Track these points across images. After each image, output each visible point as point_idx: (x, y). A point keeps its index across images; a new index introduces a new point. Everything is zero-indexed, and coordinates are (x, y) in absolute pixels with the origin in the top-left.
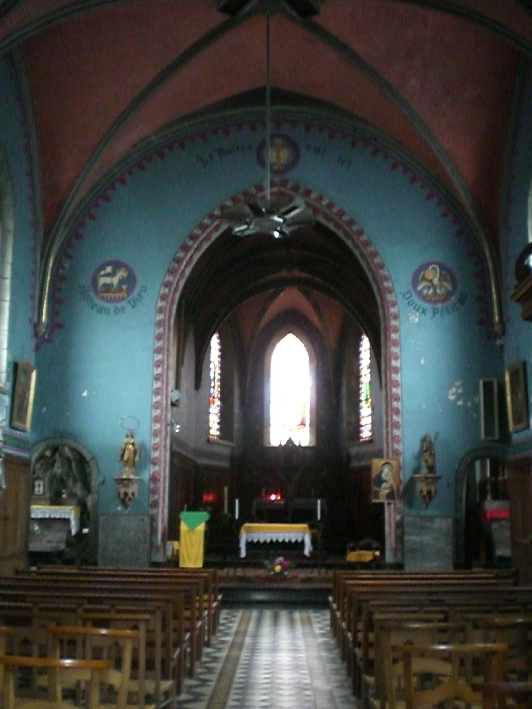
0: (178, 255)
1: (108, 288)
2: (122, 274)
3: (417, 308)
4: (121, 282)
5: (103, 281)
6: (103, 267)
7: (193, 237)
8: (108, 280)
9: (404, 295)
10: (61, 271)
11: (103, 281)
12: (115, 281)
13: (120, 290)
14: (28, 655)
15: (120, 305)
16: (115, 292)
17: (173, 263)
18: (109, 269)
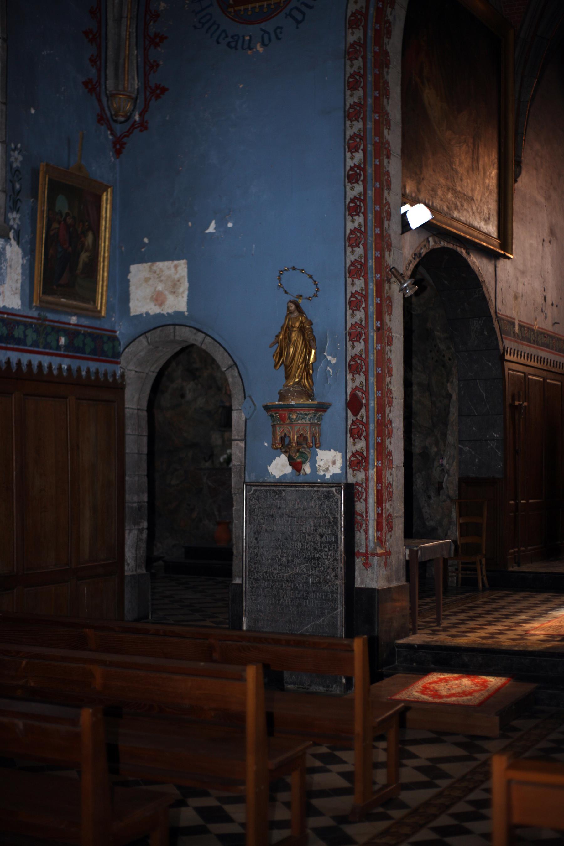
9: (298, 22)
15: (269, 26)
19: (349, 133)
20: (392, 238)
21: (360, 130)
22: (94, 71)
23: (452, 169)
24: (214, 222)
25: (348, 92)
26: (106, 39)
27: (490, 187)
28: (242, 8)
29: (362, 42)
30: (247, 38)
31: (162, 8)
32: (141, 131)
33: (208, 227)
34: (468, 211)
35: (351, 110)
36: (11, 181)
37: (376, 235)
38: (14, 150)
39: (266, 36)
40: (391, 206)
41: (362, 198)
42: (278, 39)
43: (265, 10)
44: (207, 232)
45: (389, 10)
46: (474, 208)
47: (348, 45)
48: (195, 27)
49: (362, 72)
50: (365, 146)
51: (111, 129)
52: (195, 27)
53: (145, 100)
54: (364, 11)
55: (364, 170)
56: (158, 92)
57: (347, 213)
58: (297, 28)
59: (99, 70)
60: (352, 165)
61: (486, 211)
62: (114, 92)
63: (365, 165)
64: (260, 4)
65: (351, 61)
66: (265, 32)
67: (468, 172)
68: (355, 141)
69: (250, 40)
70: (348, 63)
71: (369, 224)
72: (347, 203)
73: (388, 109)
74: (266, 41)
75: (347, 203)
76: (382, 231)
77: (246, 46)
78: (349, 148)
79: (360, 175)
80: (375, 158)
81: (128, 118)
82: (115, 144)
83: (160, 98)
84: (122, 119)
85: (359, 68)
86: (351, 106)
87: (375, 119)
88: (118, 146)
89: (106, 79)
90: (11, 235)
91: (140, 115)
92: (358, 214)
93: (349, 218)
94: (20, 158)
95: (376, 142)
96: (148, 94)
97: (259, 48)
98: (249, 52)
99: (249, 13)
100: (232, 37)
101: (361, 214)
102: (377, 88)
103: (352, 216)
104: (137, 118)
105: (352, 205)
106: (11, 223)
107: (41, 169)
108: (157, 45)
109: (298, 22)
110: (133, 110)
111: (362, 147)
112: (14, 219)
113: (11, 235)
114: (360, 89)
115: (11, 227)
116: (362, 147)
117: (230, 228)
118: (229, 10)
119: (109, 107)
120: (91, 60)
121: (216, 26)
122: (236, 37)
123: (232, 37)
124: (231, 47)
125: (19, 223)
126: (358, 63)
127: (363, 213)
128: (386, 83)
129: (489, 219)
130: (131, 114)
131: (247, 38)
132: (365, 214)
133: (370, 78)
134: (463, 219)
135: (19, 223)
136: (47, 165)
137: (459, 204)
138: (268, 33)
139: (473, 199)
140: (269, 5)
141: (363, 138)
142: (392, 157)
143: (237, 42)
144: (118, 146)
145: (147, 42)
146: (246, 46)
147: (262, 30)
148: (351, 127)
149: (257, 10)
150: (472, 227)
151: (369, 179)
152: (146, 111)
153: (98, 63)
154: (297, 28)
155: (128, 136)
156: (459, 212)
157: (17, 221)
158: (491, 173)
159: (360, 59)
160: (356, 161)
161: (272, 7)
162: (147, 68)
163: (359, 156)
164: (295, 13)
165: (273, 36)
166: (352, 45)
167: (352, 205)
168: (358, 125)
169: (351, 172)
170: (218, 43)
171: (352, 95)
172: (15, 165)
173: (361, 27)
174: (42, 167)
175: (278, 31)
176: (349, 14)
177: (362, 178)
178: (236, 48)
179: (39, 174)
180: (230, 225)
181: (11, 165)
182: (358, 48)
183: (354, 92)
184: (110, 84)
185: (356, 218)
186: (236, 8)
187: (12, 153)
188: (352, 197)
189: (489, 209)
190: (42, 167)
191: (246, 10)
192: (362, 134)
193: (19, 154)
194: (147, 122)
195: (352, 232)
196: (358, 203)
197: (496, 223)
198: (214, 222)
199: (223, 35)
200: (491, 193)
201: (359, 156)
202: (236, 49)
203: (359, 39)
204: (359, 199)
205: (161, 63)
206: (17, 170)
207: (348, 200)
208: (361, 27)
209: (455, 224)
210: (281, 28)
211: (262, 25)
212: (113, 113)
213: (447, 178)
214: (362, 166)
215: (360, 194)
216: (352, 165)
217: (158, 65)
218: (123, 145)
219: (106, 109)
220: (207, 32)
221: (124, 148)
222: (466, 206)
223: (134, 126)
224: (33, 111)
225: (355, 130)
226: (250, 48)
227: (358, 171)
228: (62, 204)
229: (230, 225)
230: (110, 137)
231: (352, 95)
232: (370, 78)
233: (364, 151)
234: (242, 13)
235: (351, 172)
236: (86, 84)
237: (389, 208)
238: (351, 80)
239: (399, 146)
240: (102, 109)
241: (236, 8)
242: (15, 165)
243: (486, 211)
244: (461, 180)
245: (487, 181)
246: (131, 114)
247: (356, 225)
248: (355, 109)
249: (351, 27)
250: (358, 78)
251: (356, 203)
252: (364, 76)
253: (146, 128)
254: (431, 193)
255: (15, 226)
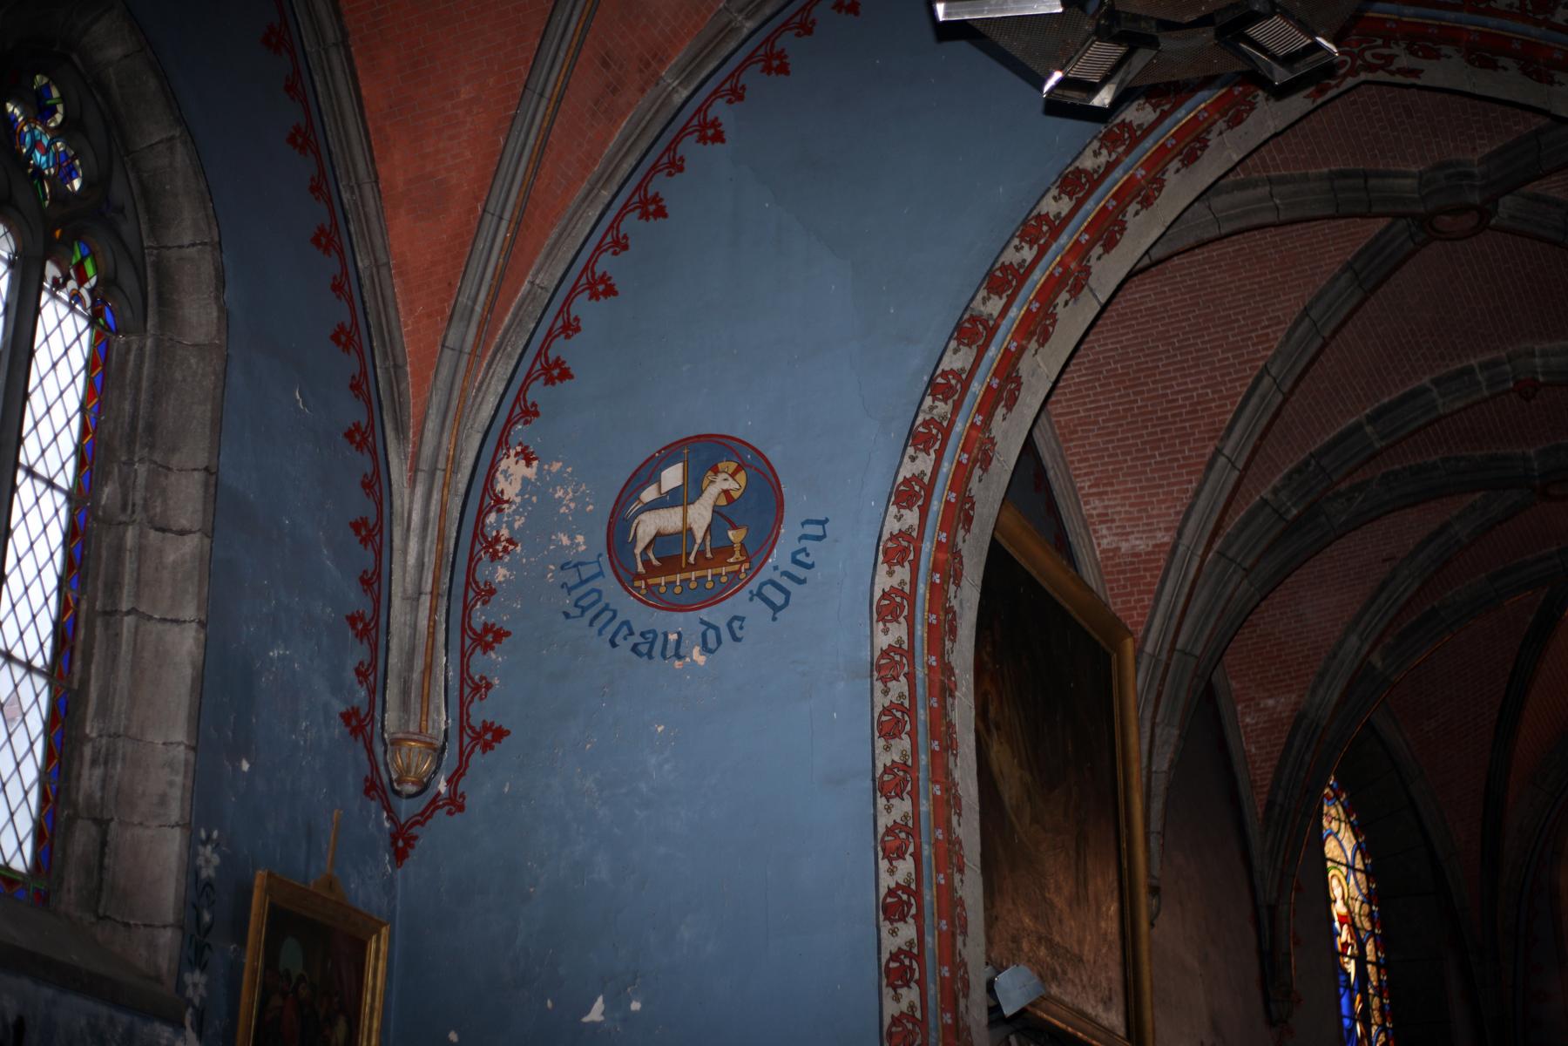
0: (945, 365)
1: (670, 552)
2: (721, 484)
3: (816, 530)
4: (722, 516)
5: (648, 526)
6: (648, 472)
7: (1003, 281)
8: (670, 520)
9: (776, 609)
10: (492, 518)
11: (648, 526)
12: (700, 515)
13: (723, 552)
14: (1485, 366)
15: (717, 615)
16: (702, 561)
17: (928, 400)
18: (672, 477)
19: (884, 821)
20: (974, 1035)
21: (905, 816)
22: (363, 693)
23: (1044, 898)
24: (600, 999)
25: (880, 743)
26: (388, 633)
27: (1110, 938)
28: (663, 580)
29: (905, 646)
30: (673, 637)
31: (501, 578)
32: (450, 813)
33: (588, 1011)
34: (1074, 985)
35: (886, 778)
36: (194, 906)
37: (945, 1026)
38: (204, 843)
39: (711, 634)
40: (970, 968)
41: (915, 951)
42: (736, 639)
43: (709, 585)
44: (585, 1019)
45: (952, 588)
46: (1085, 978)
47: (877, 653)
48: (567, 615)
49: (907, 704)
50: (918, 848)
51: (389, 809)
52: (567, 615)
53: (461, 753)
54: (907, 589)
55: (918, 894)
56: (489, 737)
57: (884, 982)
58: (774, 619)
59: (372, 692)
60: (893, 885)
61: (1104, 984)
62: (400, 735)
63: (918, 885)
64: (699, 573)
65: (885, 683)
66: (709, 625)
67: (1070, 906)
68: (897, 837)
69: (678, 642)
70: (879, 685)
71: (931, 1004)
72: (884, 961)
73: (957, 775)
74: (712, 643)
75: (884, 961)
76: (956, 1018)
77: (670, 651)
78: (884, 850)
79: (909, 905)
80: (938, 872)
81: (424, 787)
82: (394, 838)
83: (492, 748)
84: (410, 788)
85: (901, 696)
86: (886, 770)
87: (934, 795)
88: (400, 844)
89: (384, 710)
90: (188, 1018)
91: (449, 781)
92: (907, 984)
93: (888, 992)
94: (216, 860)
95: (937, 840)
96: (467, 740)
97: (698, 656)
98: (677, 664)
99: (678, 590)
100: (642, 635)
101: (913, 985)
102: (933, 736)
103: (895, 988)
104: (442, 787)
105: (893, 965)
106: (190, 992)
107: (258, 882)
108: (487, 647)
109: (776, 609)
110: (435, 773)
111: (911, 849)
112: (195, 985)
113: (188, 1018)
114: (904, 736)
115: (189, 1002)
116: (911, 849)
117: (636, 1012)
118: (637, 584)
119: (386, 765)
120: (358, 672)
121: (608, 615)
122: (650, 636)
123: (642, 635)
124: (639, 654)
125: (205, 995)
126: (900, 686)
127: (917, 982)
128: (950, 725)
129: (1110, 999)
130: (430, 779)
131: (673, 637)
132: (921, 984)
133: (922, 715)
134: (1067, 999)
135: (205, 995)
136: (270, 875)
137: (1059, 970)
138: (716, 629)
139: (1081, 960)
140: (716, 576)
141: (914, 832)
142: (966, 871)
143: (652, 644)
144: (400, 844)
145: (468, 642)
146: (670, 651)
147: (703, 622)
148: (888, 809)
149: (693, 585)
150: (1083, 1014)
151: (927, 912)
152: (462, 775)
153: (371, 678)
154: (774, 619)
155: (422, 824)
156: (1059, 986)
157: (202, 990)
158: (1108, 909)
159: (902, 678)
160: (900, 877)
161: (724, 579)
162: (467, 690)
163: (906, 867)
164: (769, 591)
165: (725, 635)
166: (885, 653)
167: (893, 965)
168: (903, 807)
169: (889, 900)
170: (613, 644)
171: (887, 748)
172: (204, 874)
173: (902, 619)
174: (260, 878)
175: (736, 624)
176: (878, 594)
177: (913, 911)
178: (650, 655)
179: (250, 893)
180: (635, 1006)
181: (197, 874)
182: (897, 658)
183: (892, 742)
184: (392, 718)
185: (903, 991)
186: (651, 581)
187: (201, 849)
188: (894, 950)
189: (1109, 979)
190: (260, 878)
191: (671, 584)
192: (910, 824)
193: (213, 851)
194: (462, 796)
195: (896, 1021)
196: (907, 962)
197: (1121, 1008)
198: (600, 999)
199: (625, 630)
200: (1110, 948)
201: (906, 867)
202: (650, 657)
203: (900, 641)
204: (909, 954)
205: (496, 681)
206: (208, 884)
207: (885, 956)
208: (902, 619)
209: (1054, 1008)
210: (742, 619)
211: (704, 614)
212: (394, 777)
213: (1036, 918)
214: (913, 886)
215: (910, 943)
216: (893, 885)
217: (489, 686)
218: (410, 841)
219: (382, 768)
220: (591, 624)
221: (412, 847)
222: (1070, 975)
223: (434, 804)
224: (245, 766)
225: (896, 815)
226: (679, 657)
227: (905, 897)
228: (292, 956)
229: (635, 1006)
230: (387, 825)
231: (887, 748)
232: (922, 715)
233: (917, 857)
234: (663, 590)
235: (889, 900)
236: (346, 717)
237: (966, 972)
238: (884, 718)
239: (978, 849)
240: (374, 767)
241: (651, 581)
242: (204, 874)
243: (1104, 984)
244: (1060, 921)
245: (1103, 924)
246: (430, 779)
247: (904, 1006)
248: (895, 775)
249: (881, 619)
250: (899, 714)
251: (902, 962)
252: (911, 711)
253: (461, 808)
254: (1011, 945)
255: (197, 1001)
